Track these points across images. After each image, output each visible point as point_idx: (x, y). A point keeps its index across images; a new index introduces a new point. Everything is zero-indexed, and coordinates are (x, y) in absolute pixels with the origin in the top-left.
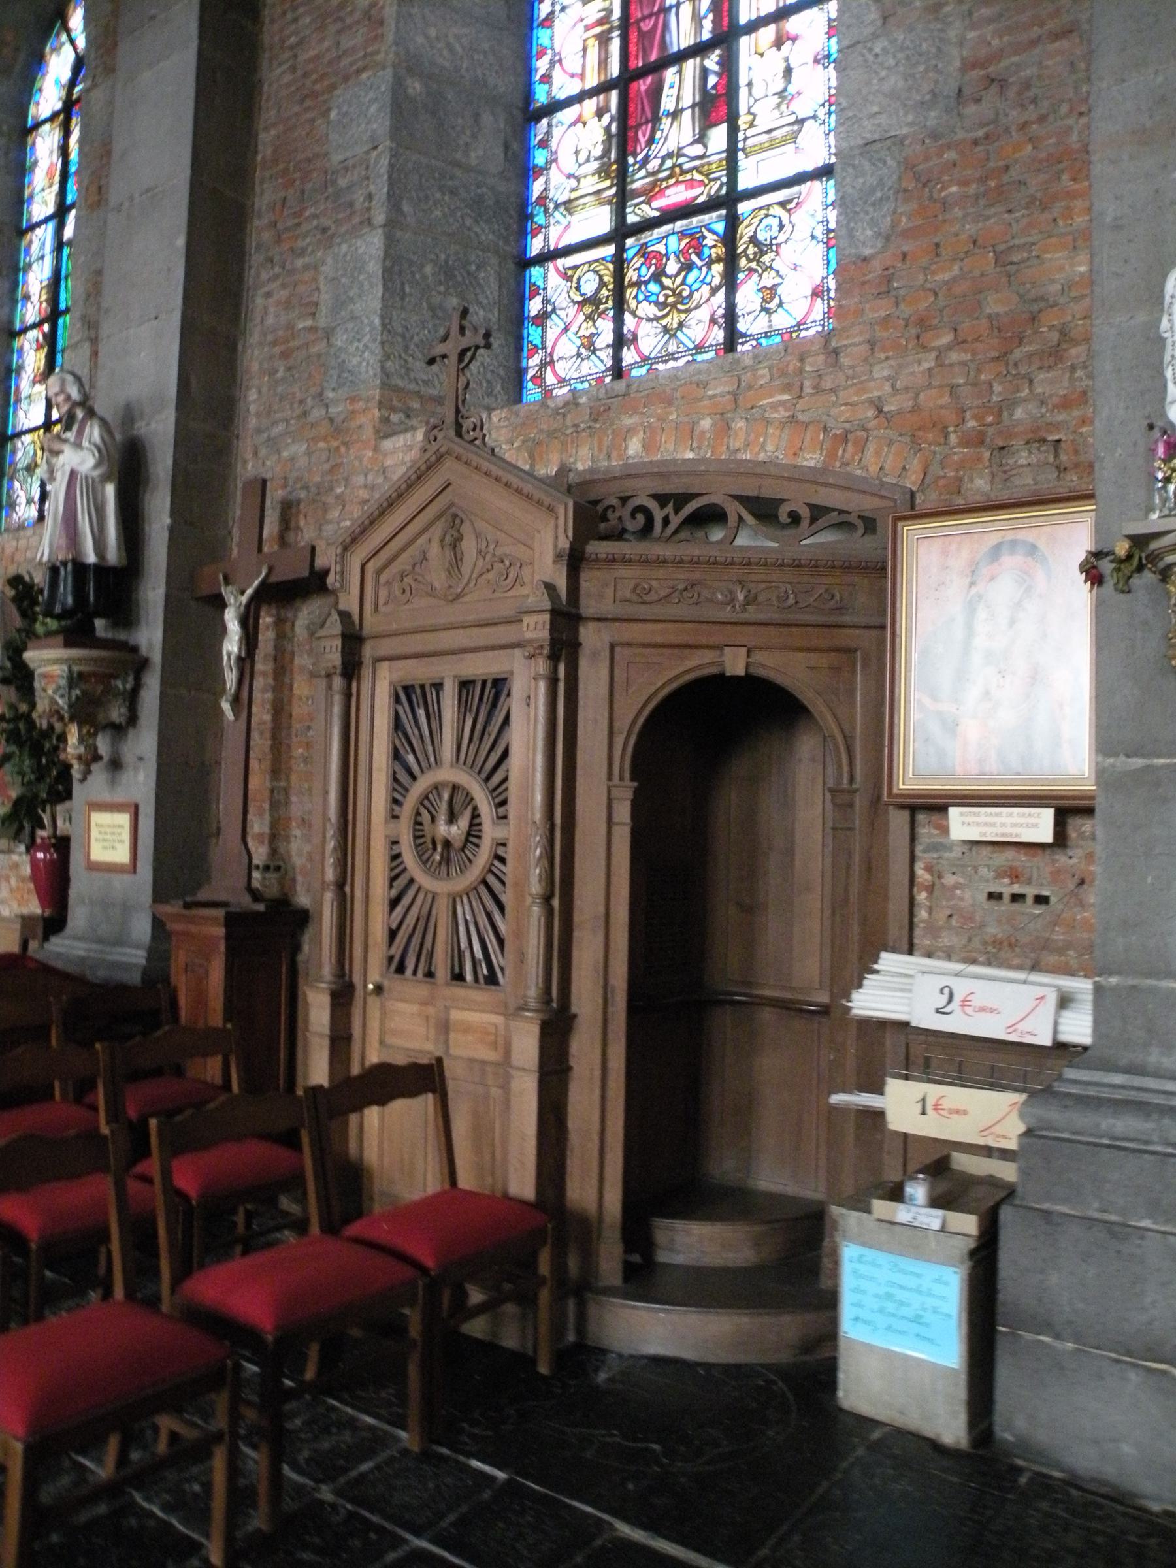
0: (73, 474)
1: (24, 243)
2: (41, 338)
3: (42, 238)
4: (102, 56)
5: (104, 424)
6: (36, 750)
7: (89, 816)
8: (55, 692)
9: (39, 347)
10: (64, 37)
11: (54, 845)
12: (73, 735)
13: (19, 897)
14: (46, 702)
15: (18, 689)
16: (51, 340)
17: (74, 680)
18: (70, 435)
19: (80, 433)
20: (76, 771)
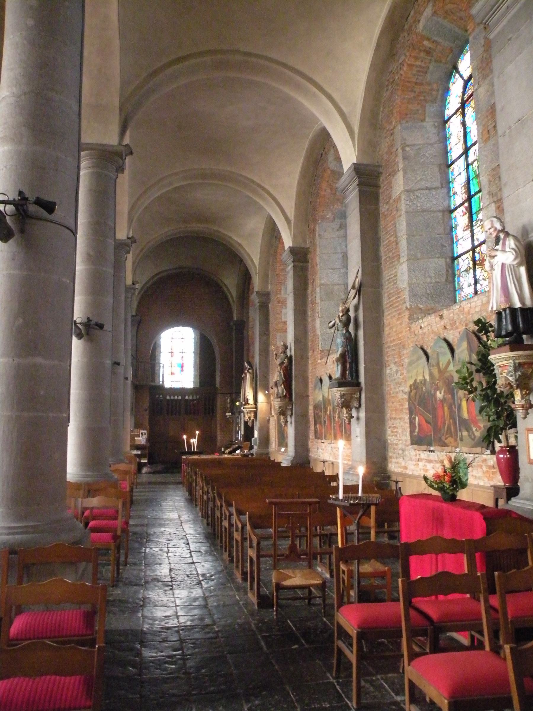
0: (503, 265)
1: (451, 170)
2: (465, 210)
3: (459, 167)
4: (481, 72)
5: (515, 238)
6: (497, 403)
7: (528, 436)
8: (507, 375)
9: (464, 214)
10: (457, 75)
11: (508, 451)
12: (518, 395)
13: (488, 475)
14: (503, 379)
15: (484, 374)
16: (470, 210)
17: (518, 367)
18: (499, 247)
19: (504, 244)
20: (520, 414)
